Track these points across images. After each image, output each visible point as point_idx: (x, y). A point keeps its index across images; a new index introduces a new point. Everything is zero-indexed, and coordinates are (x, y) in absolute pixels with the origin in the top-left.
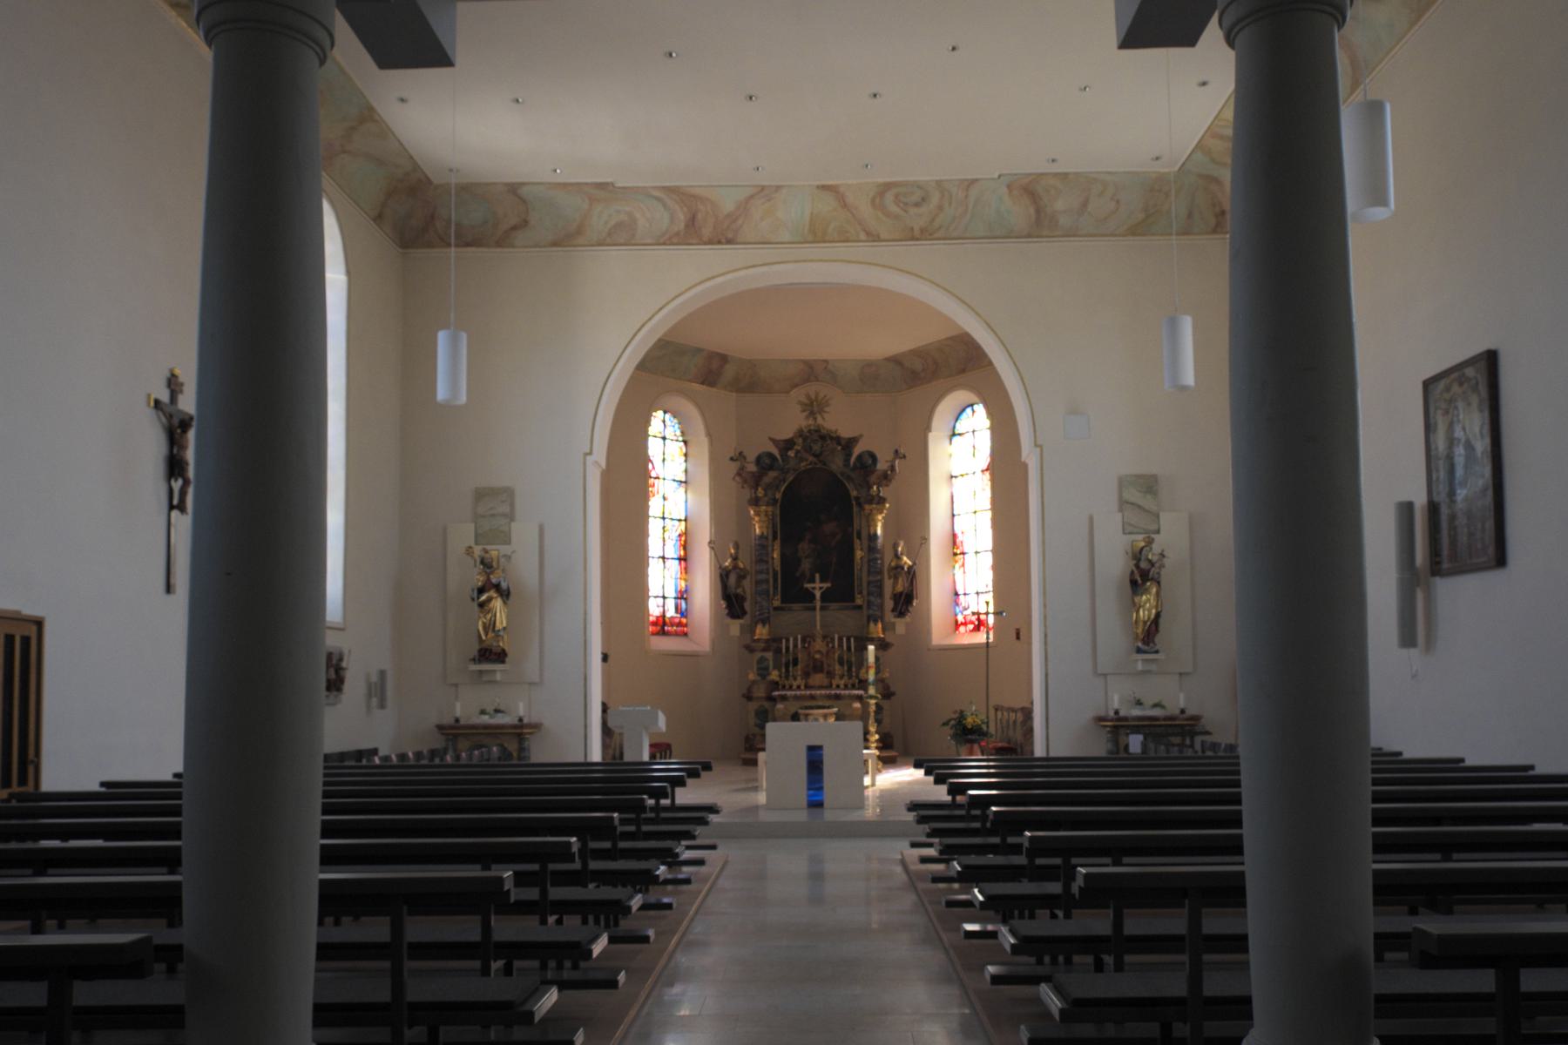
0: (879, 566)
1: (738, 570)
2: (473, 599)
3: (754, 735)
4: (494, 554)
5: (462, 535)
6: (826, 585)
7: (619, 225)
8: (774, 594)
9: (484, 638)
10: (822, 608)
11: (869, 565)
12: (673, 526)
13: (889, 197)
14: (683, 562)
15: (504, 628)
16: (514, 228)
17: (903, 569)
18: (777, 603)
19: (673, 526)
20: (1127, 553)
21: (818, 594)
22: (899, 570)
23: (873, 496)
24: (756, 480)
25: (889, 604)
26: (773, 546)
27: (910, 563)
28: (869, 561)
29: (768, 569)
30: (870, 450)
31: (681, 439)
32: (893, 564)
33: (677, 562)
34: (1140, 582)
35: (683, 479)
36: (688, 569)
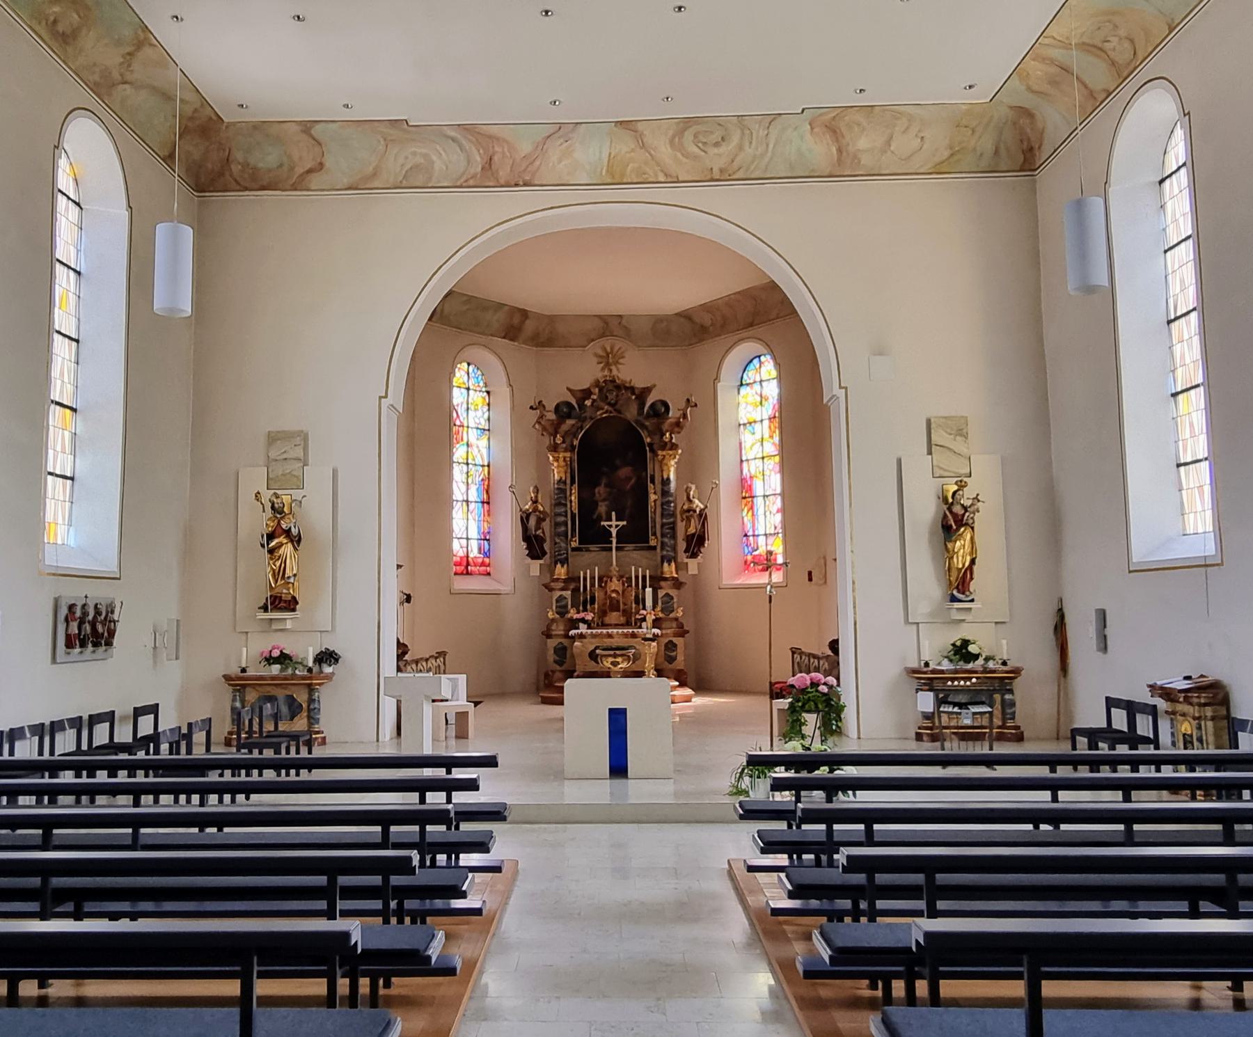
0: (672, 509)
1: (537, 513)
2: (263, 546)
3: (553, 672)
4: (286, 499)
5: (255, 480)
6: (621, 523)
7: (415, 168)
8: (573, 536)
9: (273, 585)
10: (617, 548)
11: (663, 509)
12: (477, 471)
13: (689, 136)
14: (485, 505)
15: (295, 575)
16: (310, 171)
17: (695, 511)
18: (574, 544)
19: (477, 471)
20: (939, 498)
21: (614, 532)
22: (691, 513)
23: (666, 443)
24: (555, 429)
25: (682, 545)
26: (571, 490)
27: (702, 507)
28: (662, 504)
29: (566, 512)
30: (663, 399)
31: (484, 389)
32: (685, 507)
33: (480, 505)
34: (954, 527)
35: (487, 428)
36: (491, 513)
